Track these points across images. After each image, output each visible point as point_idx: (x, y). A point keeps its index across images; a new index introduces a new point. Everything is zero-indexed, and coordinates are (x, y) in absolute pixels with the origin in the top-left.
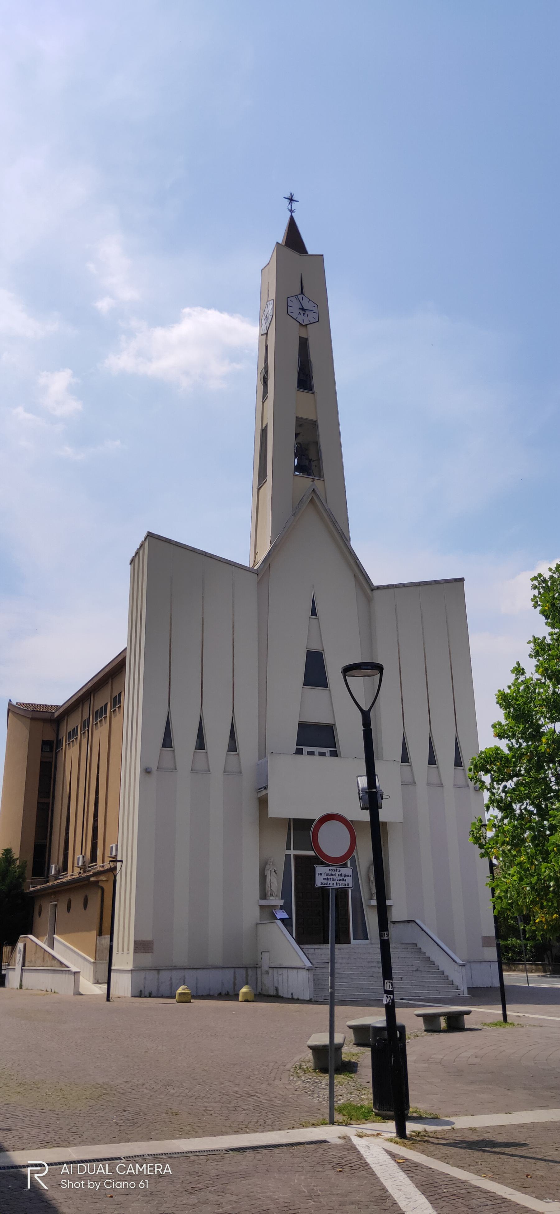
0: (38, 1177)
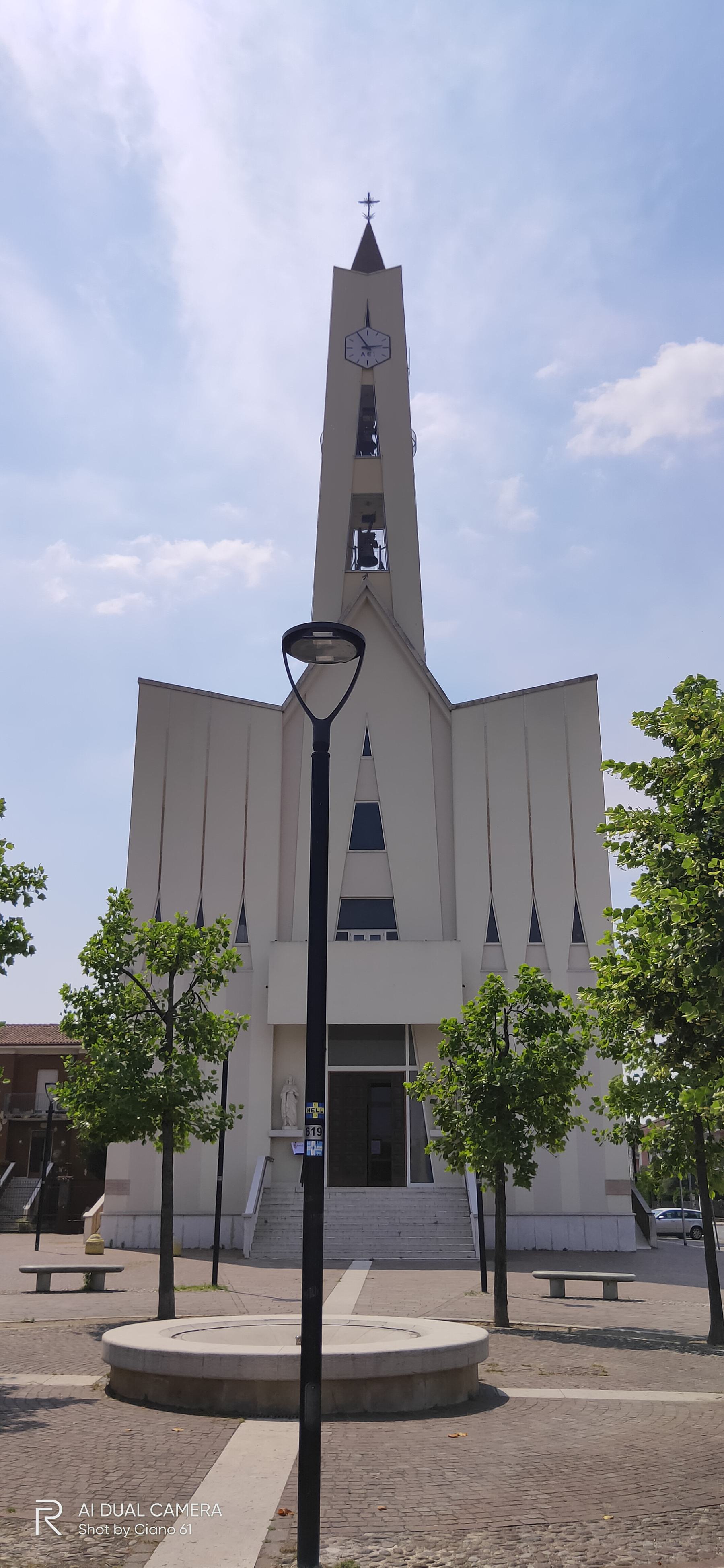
0: (50, 1520)
